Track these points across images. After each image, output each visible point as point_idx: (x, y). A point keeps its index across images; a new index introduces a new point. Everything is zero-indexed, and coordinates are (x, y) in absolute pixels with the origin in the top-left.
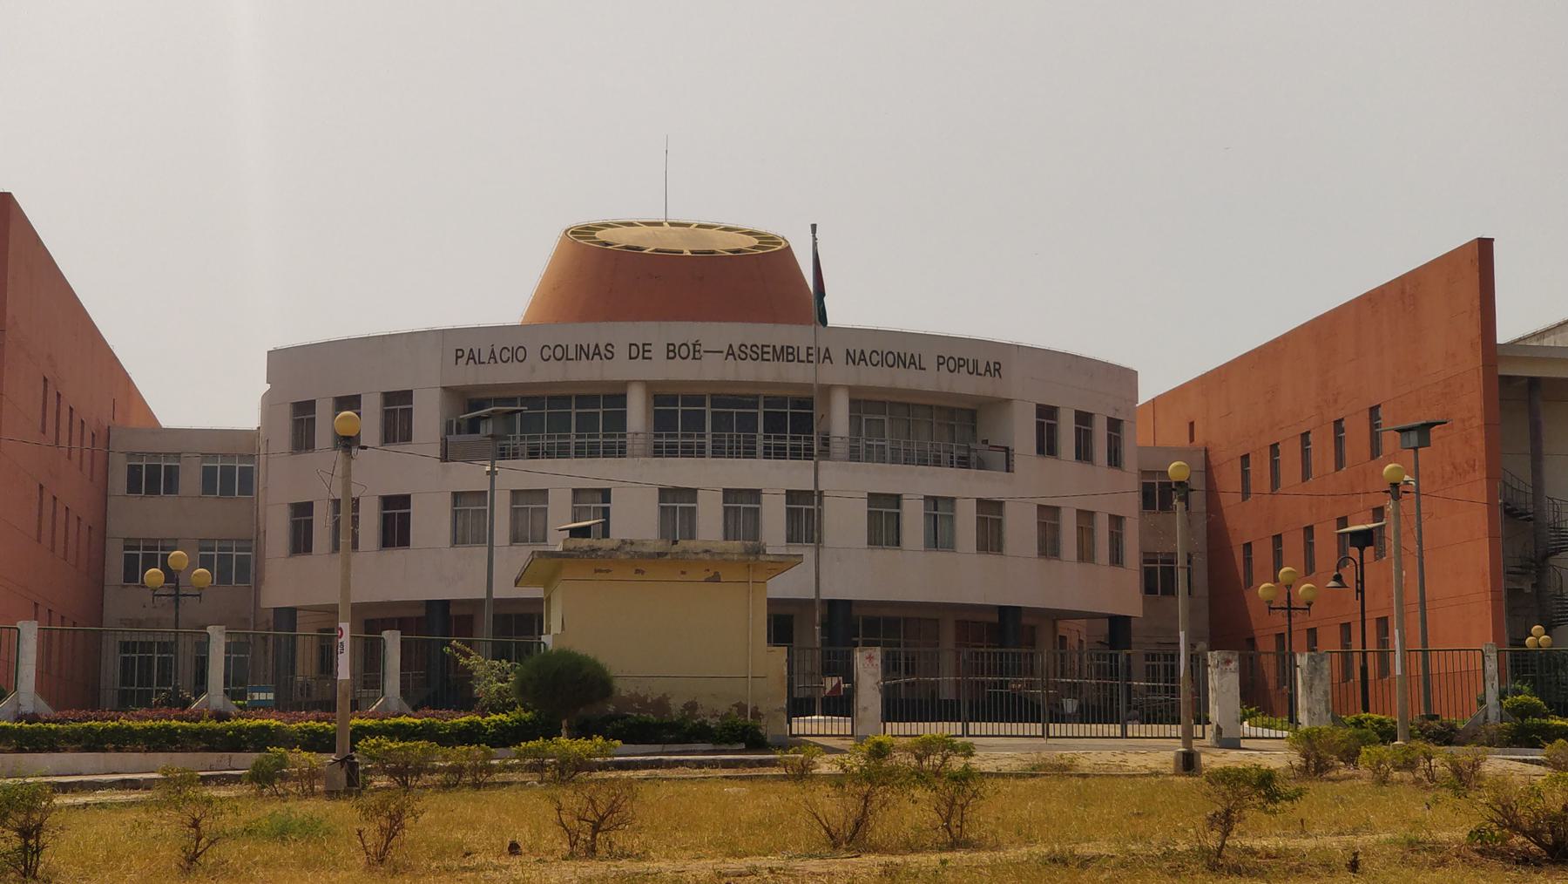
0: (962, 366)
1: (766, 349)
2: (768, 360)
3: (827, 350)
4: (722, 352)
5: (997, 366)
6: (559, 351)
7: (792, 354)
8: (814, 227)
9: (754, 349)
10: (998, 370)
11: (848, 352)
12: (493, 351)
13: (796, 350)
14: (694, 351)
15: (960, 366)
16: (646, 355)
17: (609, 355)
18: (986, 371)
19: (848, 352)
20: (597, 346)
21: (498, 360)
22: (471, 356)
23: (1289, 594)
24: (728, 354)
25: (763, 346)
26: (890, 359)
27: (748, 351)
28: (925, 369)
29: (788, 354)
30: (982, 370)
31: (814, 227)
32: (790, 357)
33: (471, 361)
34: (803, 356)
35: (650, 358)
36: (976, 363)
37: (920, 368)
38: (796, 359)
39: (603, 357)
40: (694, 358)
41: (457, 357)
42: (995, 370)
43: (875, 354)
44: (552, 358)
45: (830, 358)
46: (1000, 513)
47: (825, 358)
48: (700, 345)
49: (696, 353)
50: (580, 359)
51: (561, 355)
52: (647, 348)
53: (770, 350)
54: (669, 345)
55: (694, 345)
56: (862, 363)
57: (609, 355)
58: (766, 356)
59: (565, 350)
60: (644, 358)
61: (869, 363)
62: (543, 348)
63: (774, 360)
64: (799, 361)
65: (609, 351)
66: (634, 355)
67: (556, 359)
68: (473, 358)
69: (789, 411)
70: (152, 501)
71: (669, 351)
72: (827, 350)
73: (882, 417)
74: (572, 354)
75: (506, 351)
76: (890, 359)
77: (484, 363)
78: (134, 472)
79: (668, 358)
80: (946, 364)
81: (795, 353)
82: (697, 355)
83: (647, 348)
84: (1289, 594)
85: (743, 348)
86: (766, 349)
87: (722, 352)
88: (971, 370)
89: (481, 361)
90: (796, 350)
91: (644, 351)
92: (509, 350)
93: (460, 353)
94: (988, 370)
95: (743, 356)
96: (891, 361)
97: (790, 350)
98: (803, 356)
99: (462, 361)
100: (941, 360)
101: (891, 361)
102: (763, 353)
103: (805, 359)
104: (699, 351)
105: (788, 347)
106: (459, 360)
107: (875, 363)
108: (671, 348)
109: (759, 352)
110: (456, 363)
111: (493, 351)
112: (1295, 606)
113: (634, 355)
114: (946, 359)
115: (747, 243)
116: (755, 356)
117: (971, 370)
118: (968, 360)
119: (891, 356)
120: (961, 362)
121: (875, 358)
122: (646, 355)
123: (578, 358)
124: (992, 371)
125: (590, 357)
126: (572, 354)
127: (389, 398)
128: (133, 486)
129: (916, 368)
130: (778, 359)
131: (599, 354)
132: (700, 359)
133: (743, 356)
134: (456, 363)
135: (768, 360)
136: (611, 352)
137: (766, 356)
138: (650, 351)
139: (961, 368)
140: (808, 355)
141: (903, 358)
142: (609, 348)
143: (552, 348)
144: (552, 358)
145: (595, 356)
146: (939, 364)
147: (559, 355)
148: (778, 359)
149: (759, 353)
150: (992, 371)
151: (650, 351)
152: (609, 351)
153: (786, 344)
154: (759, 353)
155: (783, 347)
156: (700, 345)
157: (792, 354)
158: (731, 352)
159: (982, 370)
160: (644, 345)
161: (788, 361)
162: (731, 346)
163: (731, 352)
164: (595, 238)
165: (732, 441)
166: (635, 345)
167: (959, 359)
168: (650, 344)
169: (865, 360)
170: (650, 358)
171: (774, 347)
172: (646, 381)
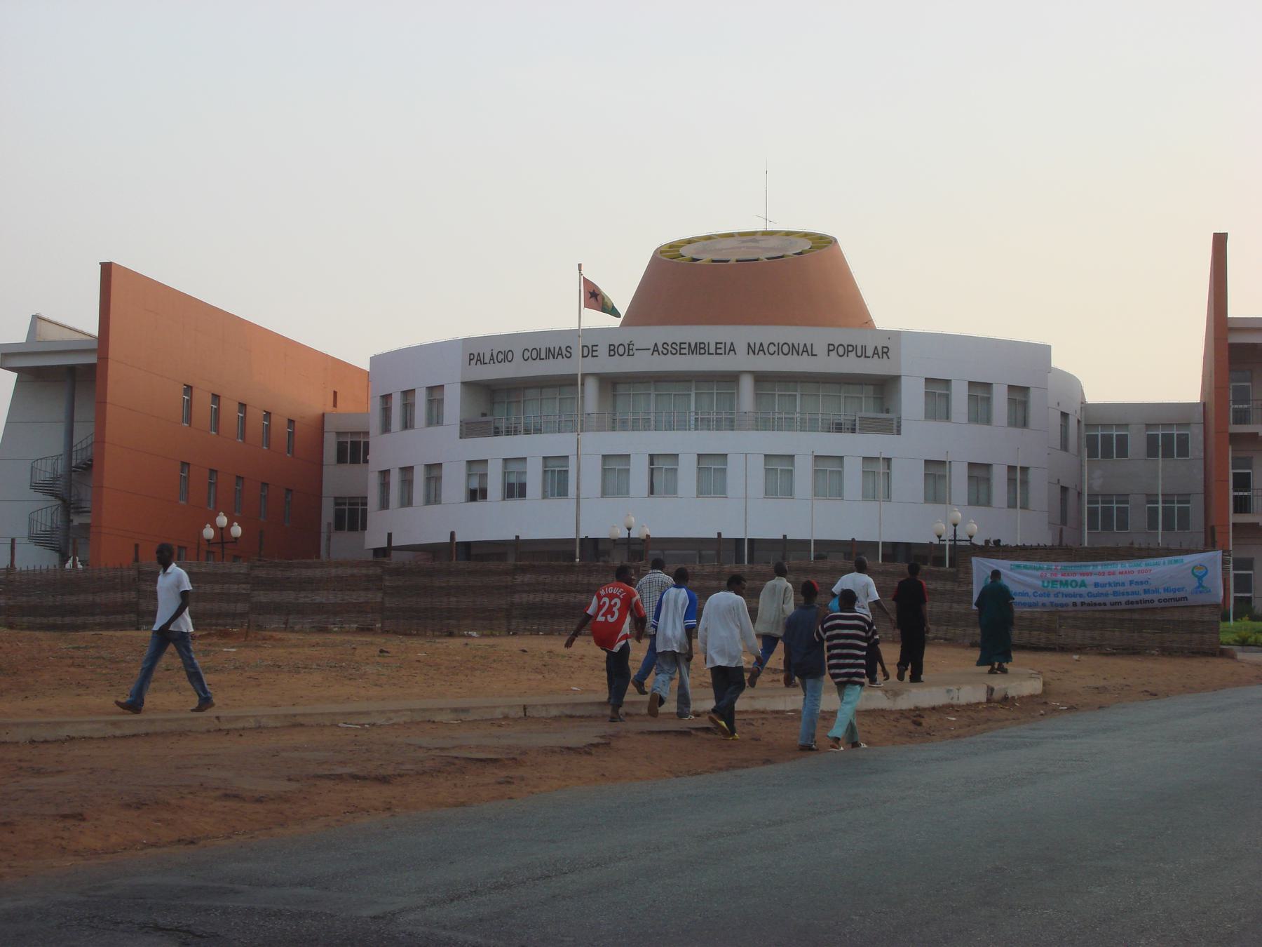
0: (831, 350)
1: (683, 346)
2: (685, 354)
3: (732, 344)
4: (649, 349)
5: (885, 350)
6: (534, 353)
7: (703, 348)
8: (580, 266)
9: (674, 346)
10: (886, 353)
11: (749, 344)
12: (492, 355)
13: (707, 346)
14: (629, 349)
15: (848, 351)
16: (595, 354)
17: (568, 355)
18: (874, 354)
19: (749, 344)
20: (560, 348)
21: (496, 361)
22: (560, 353)
23: (955, 530)
24: (654, 351)
25: (681, 343)
26: (786, 349)
27: (669, 348)
28: (816, 355)
29: (700, 348)
30: (869, 353)
31: (580, 266)
32: (702, 351)
33: (479, 362)
34: (712, 350)
35: (597, 356)
36: (864, 348)
37: (812, 355)
38: (707, 352)
39: (660, 352)
40: (628, 355)
41: (470, 360)
42: (883, 353)
43: (526, 351)
44: (530, 358)
45: (734, 350)
46: (792, 464)
47: (730, 350)
48: (633, 344)
49: (631, 351)
50: (862, 346)
51: (839, 348)
52: (595, 348)
53: (686, 346)
54: (610, 345)
55: (629, 345)
56: (805, 354)
57: (568, 355)
58: (683, 351)
59: (539, 353)
60: (680, 354)
61: (496, 361)
62: (769, 345)
63: (725, 354)
64: (709, 354)
65: (674, 349)
66: (585, 354)
67: (619, 355)
68: (480, 360)
69: (715, 391)
70: (356, 466)
71: (610, 350)
72: (732, 344)
73: (861, 396)
74: (543, 356)
75: (772, 345)
76: (786, 349)
77: (486, 363)
78: (341, 448)
79: (610, 356)
80: (854, 352)
81: (706, 348)
82: (631, 353)
83: (595, 348)
84: (955, 530)
85: (665, 346)
86: (683, 346)
87: (649, 349)
88: (859, 354)
89: (814, 353)
90: (707, 346)
91: (593, 351)
92: (775, 345)
93: (472, 357)
94: (875, 353)
95: (665, 352)
96: (786, 350)
97: (702, 346)
98: (712, 350)
99: (473, 362)
100: (831, 348)
101: (786, 350)
102: (681, 348)
103: (714, 352)
104: (632, 349)
105: (700, 343)
106: (471, 362)
107: (500, 361)
108: (612, 348)
109: (678, 348)
110: (470, 364)
111: (492, 355)
112: (960, 538)
113: (585, 354)
114: (590, 355)
115: (77, 337)
116: (674, 351)
117: (859, 354)
118: (856, 346)
119: (786, 347)
120: (850, 348)
121: (772, 349)
122: (595, 354)
123: (547, 357)
124: (880, 354)
125: (800, 354)
126: (543, 356)
127: (431, 389)
128: (341, 459)
129: (481, 363)
130: (693, 353)
131: (658, 351)
132: (633, 355)
133: (665, 352)
134: (470, 364)
135: (685, 354)
136: (664, 348)
137: (683, 351)
138: (597, 351)
139: (849, 353)
140: (717, 348)
141: (750, 350)
142: (568, 349)
143: (530, 350)
144: (530, 358)
145: (804, 353)
146: (829, 351)
147: (534, 356)
148: (693, 353)
149: (678, 349)
150: (880, 354)
151: (597, 351)
152: (674, 349)
153: (698, 341)
154: (678, 349)
155: (696, 344)
156: (633, 344)
157: (703, 348)
158: (656, 350)
159: (869, 353)
160: (593, 346)
161: (700, 354)
162: (656, 344)
163: (656, 350)
164: (810, 239)
165: (773, 422)
166: (586, 346)
167: (848, 346)
168: (597, 346)
169: (763, 350)
170: (597, 356)
171: (690, 344)
172: (753, 372)
